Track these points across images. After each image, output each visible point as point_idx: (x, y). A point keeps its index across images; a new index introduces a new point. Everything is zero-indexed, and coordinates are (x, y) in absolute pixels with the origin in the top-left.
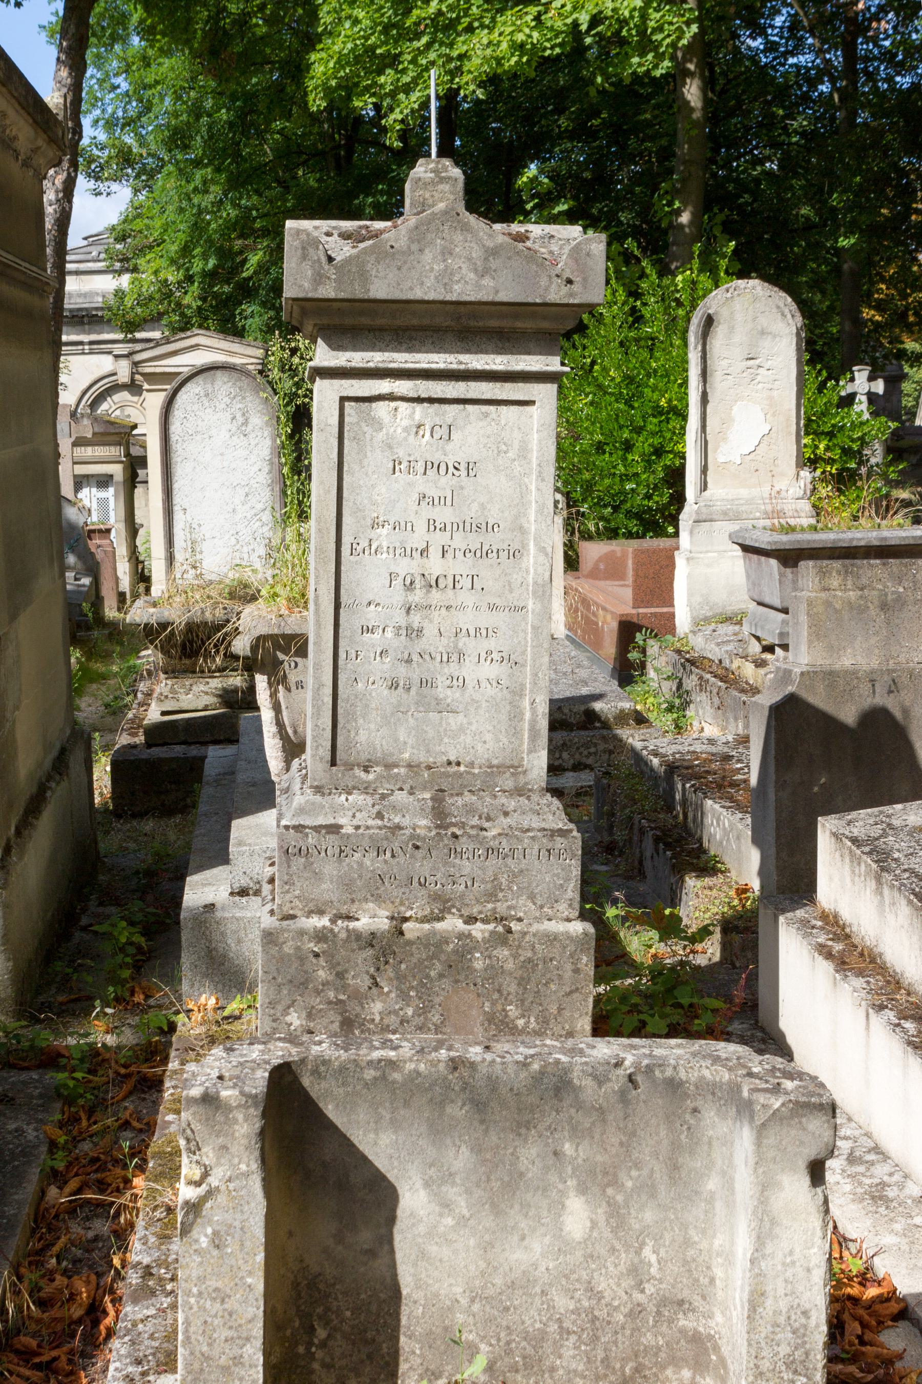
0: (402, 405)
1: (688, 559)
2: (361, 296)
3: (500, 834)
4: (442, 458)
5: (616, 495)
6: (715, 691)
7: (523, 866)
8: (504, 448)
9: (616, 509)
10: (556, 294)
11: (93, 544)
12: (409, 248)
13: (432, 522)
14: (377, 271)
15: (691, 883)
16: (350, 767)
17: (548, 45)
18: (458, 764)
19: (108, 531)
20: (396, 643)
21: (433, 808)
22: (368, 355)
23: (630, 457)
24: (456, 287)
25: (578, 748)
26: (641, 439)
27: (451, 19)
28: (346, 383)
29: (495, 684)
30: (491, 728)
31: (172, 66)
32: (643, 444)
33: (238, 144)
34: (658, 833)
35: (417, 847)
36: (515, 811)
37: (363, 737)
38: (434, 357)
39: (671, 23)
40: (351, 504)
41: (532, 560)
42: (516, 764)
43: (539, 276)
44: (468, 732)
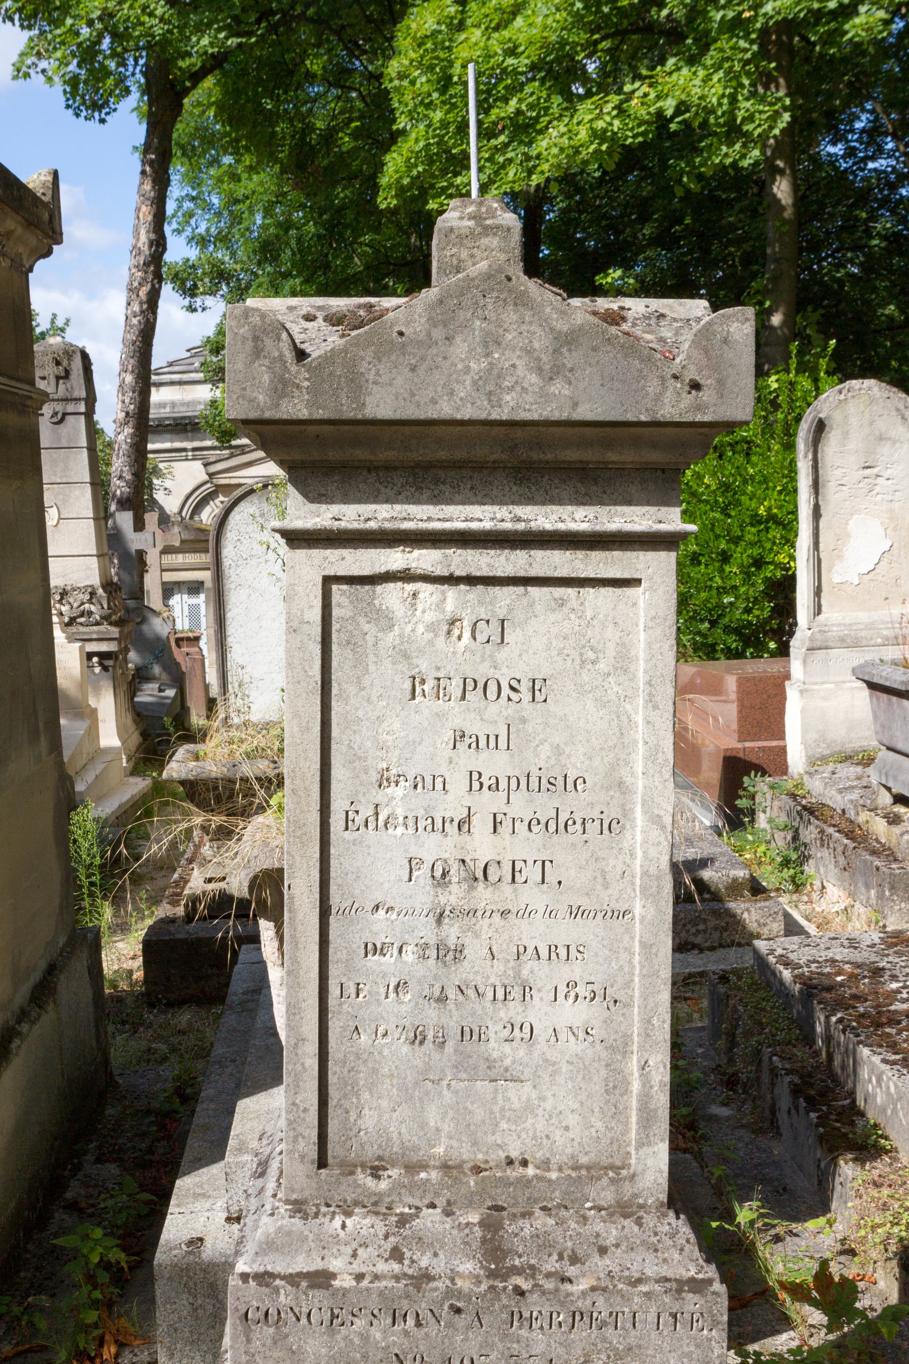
0: (426, 589)
1: (801, 692)
2: (351, 415)
3: (593, 1289)
4: (491, 673)
5: (714, 609)
6: (840, 849)
7: (632, 1341)
8: (591, 655)
9: (713, 623)
10: (674, 406)
11: (178, 654)
12: (429, 335)
13: (475, 776)
14: (377, 374)
15: (848, 1170)
16: (349, 1169)
17: (630, 134)
18: (525, 1163)
19: (197, 639)
20: (420, 970)
21: (484, 1241)
22: (367, 509)
23: (727, 569)
24: (508, 398)
25: (684, 925)
26: (739, 549)
27: (531, 118)
28: (333, 554)
29: (582, 1035)
30: (576, 1106)
31: (261, 182)
32: (741, 555)
33: (326, 255)
34: (797, 1080)
35: (458, 1311)
36: (617, 1246)
37: (369, 1121)
38: (476, 510)
39: (761, 112)
40: (344, 749)
41: (639, 838)
42: (618, 1163)
43: (645, 378)
44: (540, 1112)
